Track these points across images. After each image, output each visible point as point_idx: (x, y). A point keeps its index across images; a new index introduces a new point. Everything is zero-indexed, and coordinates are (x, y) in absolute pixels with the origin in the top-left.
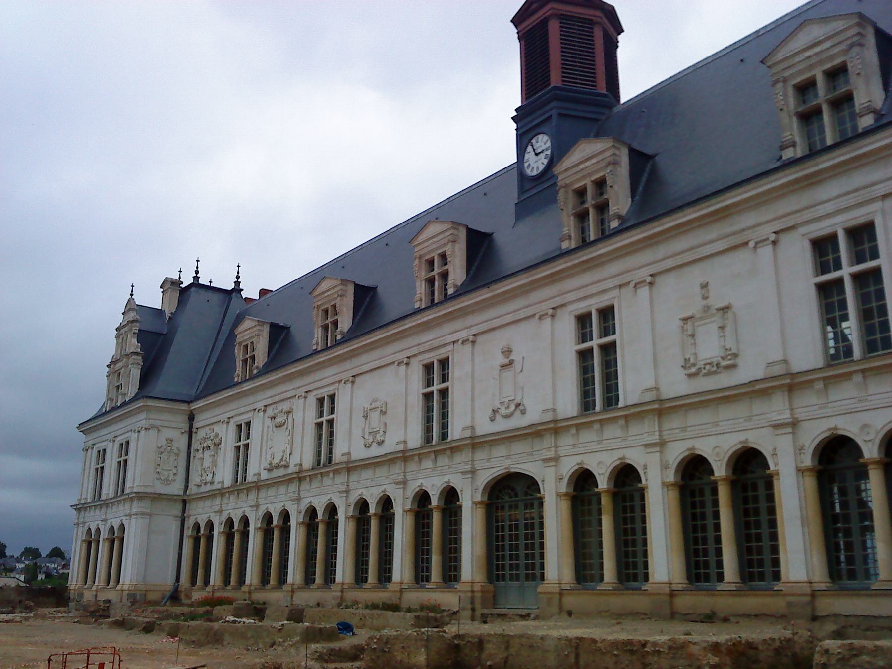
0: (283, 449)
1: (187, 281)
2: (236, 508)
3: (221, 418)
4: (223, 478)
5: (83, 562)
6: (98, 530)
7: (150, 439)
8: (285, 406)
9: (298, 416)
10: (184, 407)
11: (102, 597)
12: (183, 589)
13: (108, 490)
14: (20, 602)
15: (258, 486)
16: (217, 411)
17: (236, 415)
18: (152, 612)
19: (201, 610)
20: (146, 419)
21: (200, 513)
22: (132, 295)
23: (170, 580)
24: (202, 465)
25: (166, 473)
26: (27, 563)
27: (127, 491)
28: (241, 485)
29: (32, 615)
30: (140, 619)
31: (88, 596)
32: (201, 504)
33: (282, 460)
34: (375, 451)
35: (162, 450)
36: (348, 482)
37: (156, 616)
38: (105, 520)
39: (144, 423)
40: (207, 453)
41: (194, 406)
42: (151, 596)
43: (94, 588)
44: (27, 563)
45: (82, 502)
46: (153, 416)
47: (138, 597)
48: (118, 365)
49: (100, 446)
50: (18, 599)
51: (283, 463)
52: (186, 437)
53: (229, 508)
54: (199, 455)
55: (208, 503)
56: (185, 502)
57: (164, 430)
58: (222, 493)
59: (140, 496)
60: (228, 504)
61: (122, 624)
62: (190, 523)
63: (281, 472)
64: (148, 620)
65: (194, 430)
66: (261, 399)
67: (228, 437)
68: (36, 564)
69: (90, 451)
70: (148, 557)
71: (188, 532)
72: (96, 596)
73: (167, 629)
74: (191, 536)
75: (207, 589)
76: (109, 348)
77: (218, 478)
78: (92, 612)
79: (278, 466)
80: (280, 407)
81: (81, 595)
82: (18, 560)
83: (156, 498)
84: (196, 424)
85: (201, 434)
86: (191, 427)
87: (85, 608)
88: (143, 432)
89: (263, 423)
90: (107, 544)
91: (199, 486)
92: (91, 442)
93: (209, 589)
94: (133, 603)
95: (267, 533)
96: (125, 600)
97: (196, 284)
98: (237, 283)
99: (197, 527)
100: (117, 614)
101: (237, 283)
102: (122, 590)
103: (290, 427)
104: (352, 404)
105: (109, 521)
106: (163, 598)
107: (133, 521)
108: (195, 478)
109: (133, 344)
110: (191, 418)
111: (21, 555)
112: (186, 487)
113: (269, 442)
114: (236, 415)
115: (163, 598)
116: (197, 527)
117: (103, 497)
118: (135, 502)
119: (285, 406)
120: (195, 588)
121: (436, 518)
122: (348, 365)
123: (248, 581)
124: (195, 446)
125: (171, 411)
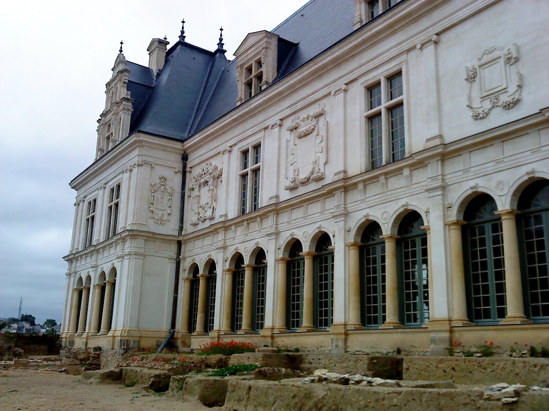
0: (313, 159)
1: (173, 40)
2: (243, 242)
3: (221, 149)
4: (226, 211)
5: (74, 311)
6: (89, 278)
7: (140, 175)
8: (314, 110)
9: (335, 109)
10: (178, 145)
11: (92, 344)
12: (179, 336)
13: (99, 234)
14: (9, 348)
16: (215, 143)
18: (155, 360)
19: (214, 358)
20: (138, 155)
21: (198, 254)
22: (121, 51)
23: (165, 326)
24: (199, 203)
26: (48, 329)
27: (119, 230)
29: (13, 363)
30: (146, 371)
31: (79, 344)
32: (198, 243)
33: (312, 173)
34: (499, 118)
35: (155, 188)
36: (443, 175)
37: (167, 366)
38: (95, 267)
39: (136, 160)
40: (205, 190)
41: (188, 144)
42: (145, 344)
43: (85, 335)
44: (48, 329)
45: (74, 252)
46: (145, 151)
48: (108, 117)
49: (90, 198)
50: (6, 346)
51: (315, 175)
52: (179, 177)
53: (237, 241)
54: (195, 193)
55: (208, 241)
56: (179, 243)
58: (227, 225)
59: (133, 234)
60: (234, 238)
61: (116, 377)
62: (186, 265)
63: (313, 186)
64: (157, 372)
65: (188, 169)
66: (273, 115)
67: (231, 167)
68: (53, 329)
69: (81, 204)
70: (142, 301)
71: (184, 275)
72: (87, 343)
73: (198, 389)
74: (187, 279)
75: (211, 334)
76: (100, 104)
77: (217, 214)
78: (82, 360)
79: (305, 183)
80: (303, 115)
81: (72, 343)
82: (42, 327)
84: (189, 165)
85: (197, 171)
86: (185, 166)
87: (75, 355)
88: (135, 170)
89: (280, 139)
90: (98, 291)
91: (195, 225)
92: (82, 196)
94: (126, 350)
96: (117, 347)
97: (182, 43)
98: (221, 44)
99: (195, 268)
100: (110, 365)
101: (221, 44)
102: (114, 337)
103: (323, 133)
104: (437, 71)
105: (100, 267)
106: (158, 346)
107: (126, 262)
108: (190, 217)
109: (123, 92)
110: (185, 158)
111: (44, 325)
112: (181, 228)
113: (291, 158)
115: (158, 346)
116: (195, 268)
117: (94, 243)
118: (128, 243)
119: (314, 110)
120: (195, 333)
121: (202, 283)
122: (424, 23)
124: (188, 185)
125: (165, 149)
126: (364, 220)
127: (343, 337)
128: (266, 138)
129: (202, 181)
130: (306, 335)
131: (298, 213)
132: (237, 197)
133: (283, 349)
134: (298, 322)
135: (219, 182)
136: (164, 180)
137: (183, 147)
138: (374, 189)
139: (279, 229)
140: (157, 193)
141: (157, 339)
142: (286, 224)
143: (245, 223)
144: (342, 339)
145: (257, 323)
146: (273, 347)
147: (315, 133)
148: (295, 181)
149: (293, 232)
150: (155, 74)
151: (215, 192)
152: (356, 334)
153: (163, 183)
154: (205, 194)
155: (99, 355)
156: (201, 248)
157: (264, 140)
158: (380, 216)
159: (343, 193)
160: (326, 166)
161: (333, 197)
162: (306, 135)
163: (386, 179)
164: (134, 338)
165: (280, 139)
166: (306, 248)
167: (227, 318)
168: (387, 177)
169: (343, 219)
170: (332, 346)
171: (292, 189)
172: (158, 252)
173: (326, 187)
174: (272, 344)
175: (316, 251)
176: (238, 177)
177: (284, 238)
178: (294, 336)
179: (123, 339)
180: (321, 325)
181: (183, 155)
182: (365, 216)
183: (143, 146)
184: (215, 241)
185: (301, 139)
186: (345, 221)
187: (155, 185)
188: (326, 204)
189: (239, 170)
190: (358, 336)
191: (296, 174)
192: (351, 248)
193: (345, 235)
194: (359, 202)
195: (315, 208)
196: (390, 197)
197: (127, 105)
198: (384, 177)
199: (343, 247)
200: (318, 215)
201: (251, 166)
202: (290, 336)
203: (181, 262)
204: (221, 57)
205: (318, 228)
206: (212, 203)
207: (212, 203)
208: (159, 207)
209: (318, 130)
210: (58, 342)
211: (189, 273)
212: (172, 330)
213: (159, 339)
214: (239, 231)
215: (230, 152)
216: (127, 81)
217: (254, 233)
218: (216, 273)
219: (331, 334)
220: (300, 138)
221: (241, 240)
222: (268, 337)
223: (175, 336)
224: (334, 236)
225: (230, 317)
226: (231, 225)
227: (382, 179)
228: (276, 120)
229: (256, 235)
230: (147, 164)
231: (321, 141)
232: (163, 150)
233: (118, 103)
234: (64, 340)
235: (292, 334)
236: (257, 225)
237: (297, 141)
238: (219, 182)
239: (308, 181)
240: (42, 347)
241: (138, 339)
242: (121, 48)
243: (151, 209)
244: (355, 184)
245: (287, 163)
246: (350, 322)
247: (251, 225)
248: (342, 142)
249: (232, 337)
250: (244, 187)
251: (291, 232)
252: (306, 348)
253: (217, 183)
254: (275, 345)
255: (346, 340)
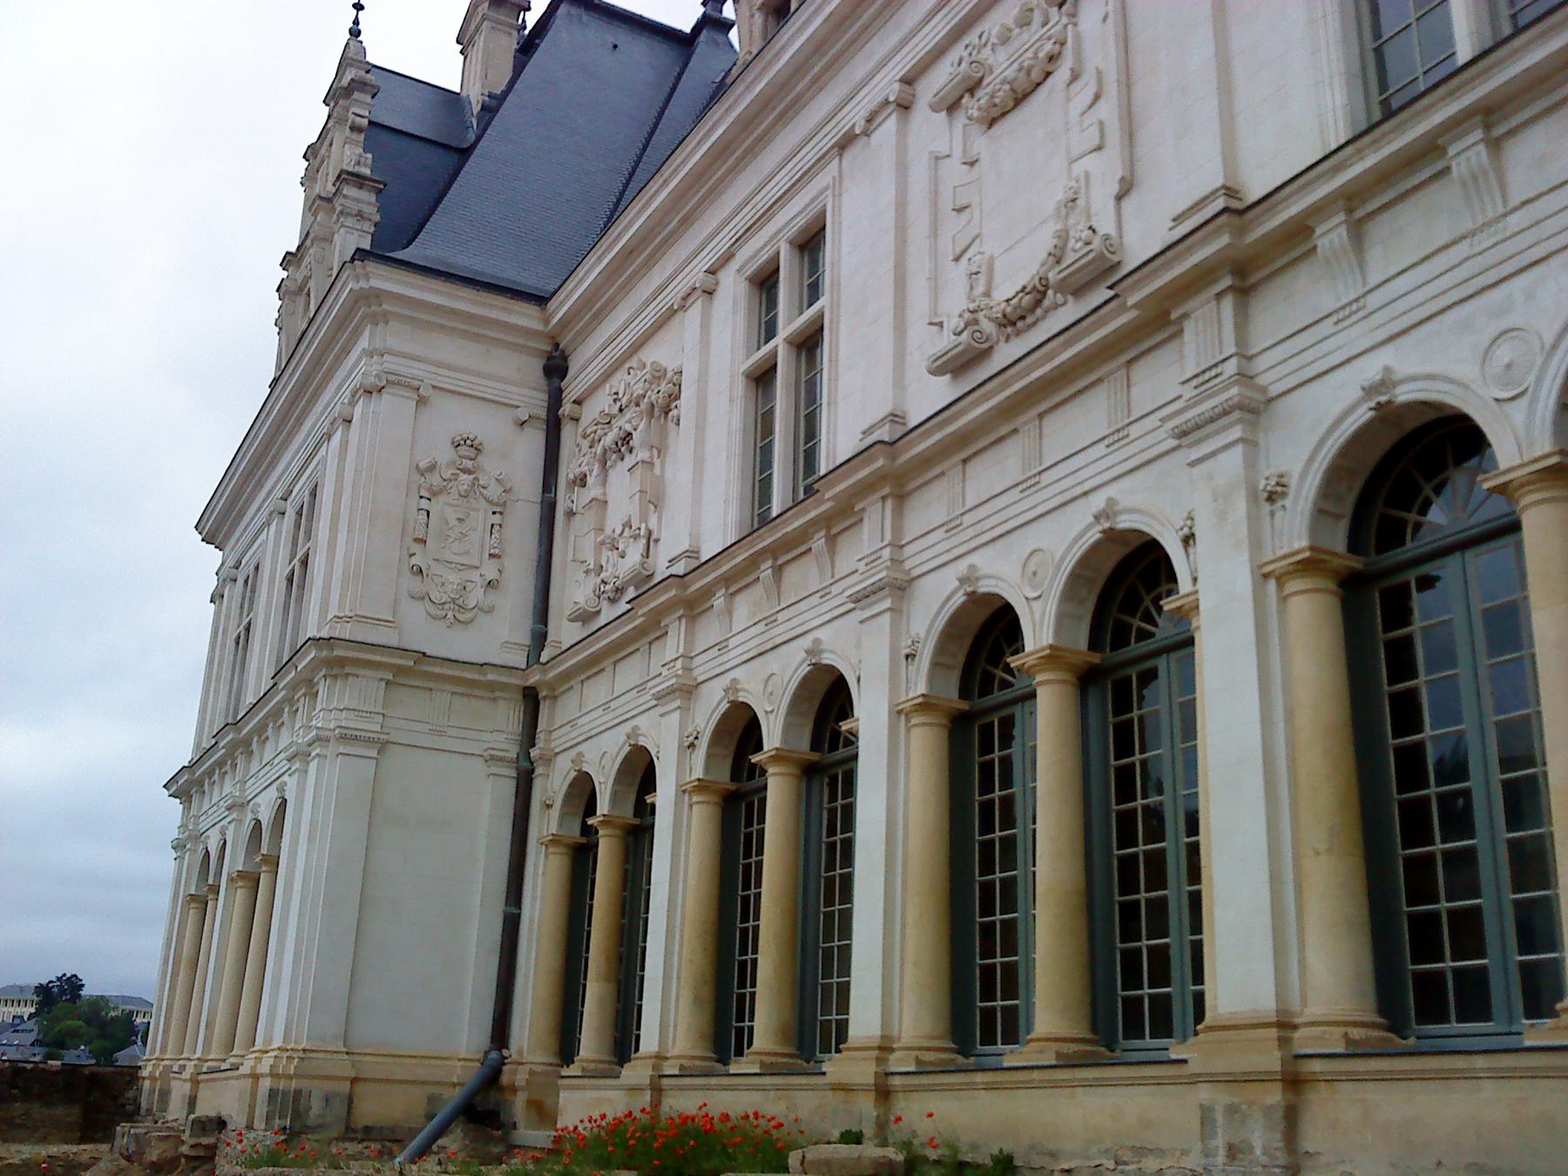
10: (524, 316)
12: (521, 1078)
15: (902, 465)
17: (739, 241)
21: (591, 735)
23: (466, 1038)
25: (454, 578)
28: (801, 502)
32: (597, 690)
33: (1057, 257)
35: (435, 480)
42: (374, 1108)
46: (394, 337)
47: (316, 1106)
52: (533, 443)
53: (735, 655)
54: (593, 490)
56: (531, 700)
57: (441, 403)
60: (722, 646)
62: (552, 785)
65: (567, 408)
67: (710, 351)
74: (555, 841)
83: (411, 670)
84: (573, 387)
86: (555, 399)
91: (585, 617)
93: (636, 1072)
94: (293, 1134)
95: (737, 808)
99: (583, 792)
102: (255, 1077)
109: (349, 154)
110: (556, 368)
112: (540, 639)
113: (953, 226)
114: (739, 241)
116: (583, 792)
120: (573, 1070)
123: (864, 1020)
124: (568, 469)
125: (472, 329)
126: (1363, 415)
127: (1274, 1096)
128: (847, 182)
129: (609, 440)
130: (1055, 1085)
131: (993, 472)
132: (735, 472)
133: (933, 1154)
134: (1011, 1015)
135: (671, 426)
136: (472, 453)
137: (547, 322)
138: (1412, 231)
139: (908, 565)
140: (442, 498)
141: (430, 1090)
142: (940, 534)
143: (766, 570)
144: (1268, 1110)
145: (817, 1027)
146: (884, 1143)
147: (1062, 74)
148: (976, 322)
149: (972, 567)
150: (476, 109)
151: (657, 471)
152: (1356, 1078)
153: (469, 464)
154: (622, 488)
155: (212, 1149)
156: (606, 706)
157: (838, 196)
158: (1467, 370)
159: (1228, 305)
160: (1129, 204)
161: (1173, 345)
162: (1020, 98)
163: (1495, 145)
164: (328, 1086)
165: (902, 168)
166: (1039, 629)
167: (697, 1000)
168: (1498, 131)
169: (1236, 433)
170: (1207, 1153)
171: (956, 365)
172: (441, 733)
173: (1133, 288)
174: (881, 1125)
175: (1095, 643)
176: (740, 383)
177: (935, 603)
178: (989, 1087)
179: (282, 1085)
180: (1134, 1030)
181: (550, 358)
182: (1369, 391)
183: (385, 317)
184: (655, 668)
185: (999, 128)
186: (1249, 443)
187: (432, 467)
188: (1135, 391)
189: (742, 352)
190: (1373, 1093)
191: (980, 289)
192: (1293, 585)
193: (1253, 520)
194: (1327, 327)
195: (1081, 422)
196: (1530, 237)
197: (358, 201)
198: (1478, 134)
199: (1243, 581)
200: (1101, 449)
201: (789, 324)
202: (972, 1087)
203: (539, 770)
204: (717, 43)
205: (1097, 517)
206: (644, 518)
207: (644, 518)
208: (449, 556)
209: (1078, 54)
210: (130, 1094)
211: (563, 816)
212: (494, 1055)
213: (436, 1090)
214: (745, 608)
215: (710, 293)
216: (365, 122)
217: (803, 606)
218: (653, 806)
219: (1195, 1080)
220: (992, 123)
221: (753, 646)
222: (864, 1089)
223: (505, 1079)
224: (1188, 540)
225: (707, 993)
226: (707, 592)
227: (1468, 154)
228: (887, 85)
229: (811, 613)
230: (399, 384)
231: (1097, 97)
232: (466, 335)
233: (329, 200)
234: (147, 1084)
235: (979, 1078)
236: (814, 572)
237: (981, 144)
238: (671, 426)
239: (1038, 303)
240: (59, 1111)
241: (345, 1087)
242: (356, 22)
243: (414, 561)
244: (1299, 233)
245: (934, 253)
246: (1315, 1010)
247: (792, 574)
248: (1202, 51)
249: (709, 1088)
250: (764, 425)
251: (961, 567)
252: (1053, 1155)
253: (663, 435)
254: (897, 1133)
255: (1291, 1119)
